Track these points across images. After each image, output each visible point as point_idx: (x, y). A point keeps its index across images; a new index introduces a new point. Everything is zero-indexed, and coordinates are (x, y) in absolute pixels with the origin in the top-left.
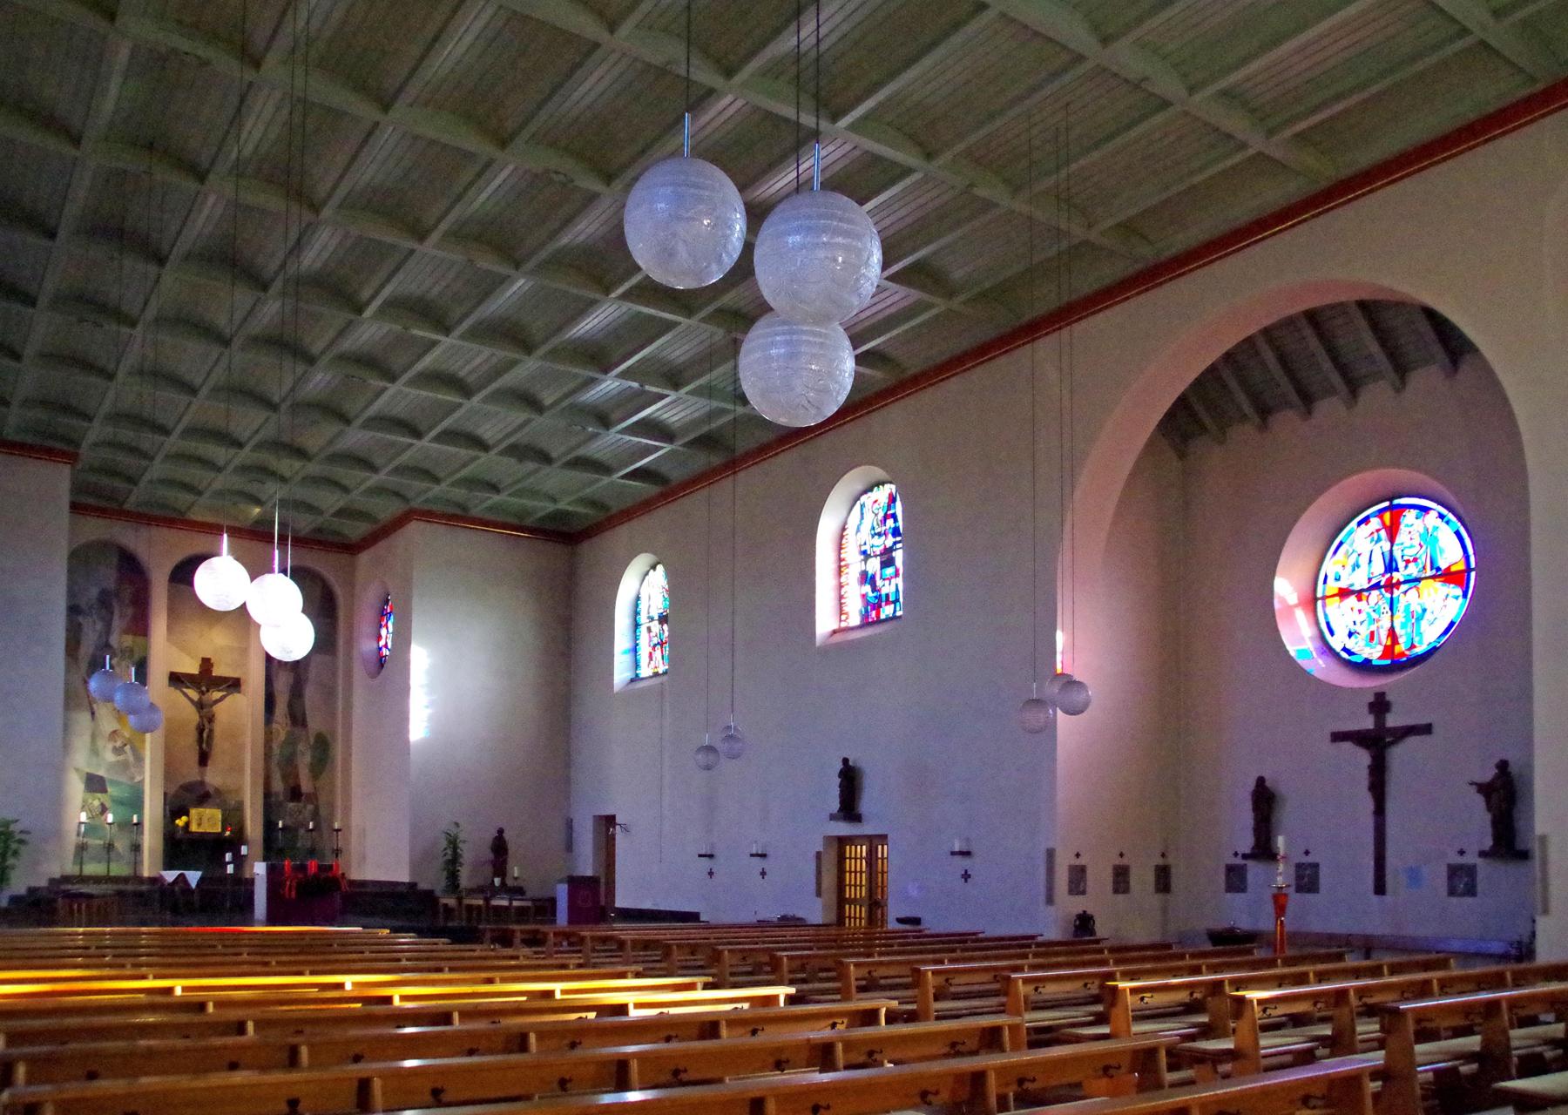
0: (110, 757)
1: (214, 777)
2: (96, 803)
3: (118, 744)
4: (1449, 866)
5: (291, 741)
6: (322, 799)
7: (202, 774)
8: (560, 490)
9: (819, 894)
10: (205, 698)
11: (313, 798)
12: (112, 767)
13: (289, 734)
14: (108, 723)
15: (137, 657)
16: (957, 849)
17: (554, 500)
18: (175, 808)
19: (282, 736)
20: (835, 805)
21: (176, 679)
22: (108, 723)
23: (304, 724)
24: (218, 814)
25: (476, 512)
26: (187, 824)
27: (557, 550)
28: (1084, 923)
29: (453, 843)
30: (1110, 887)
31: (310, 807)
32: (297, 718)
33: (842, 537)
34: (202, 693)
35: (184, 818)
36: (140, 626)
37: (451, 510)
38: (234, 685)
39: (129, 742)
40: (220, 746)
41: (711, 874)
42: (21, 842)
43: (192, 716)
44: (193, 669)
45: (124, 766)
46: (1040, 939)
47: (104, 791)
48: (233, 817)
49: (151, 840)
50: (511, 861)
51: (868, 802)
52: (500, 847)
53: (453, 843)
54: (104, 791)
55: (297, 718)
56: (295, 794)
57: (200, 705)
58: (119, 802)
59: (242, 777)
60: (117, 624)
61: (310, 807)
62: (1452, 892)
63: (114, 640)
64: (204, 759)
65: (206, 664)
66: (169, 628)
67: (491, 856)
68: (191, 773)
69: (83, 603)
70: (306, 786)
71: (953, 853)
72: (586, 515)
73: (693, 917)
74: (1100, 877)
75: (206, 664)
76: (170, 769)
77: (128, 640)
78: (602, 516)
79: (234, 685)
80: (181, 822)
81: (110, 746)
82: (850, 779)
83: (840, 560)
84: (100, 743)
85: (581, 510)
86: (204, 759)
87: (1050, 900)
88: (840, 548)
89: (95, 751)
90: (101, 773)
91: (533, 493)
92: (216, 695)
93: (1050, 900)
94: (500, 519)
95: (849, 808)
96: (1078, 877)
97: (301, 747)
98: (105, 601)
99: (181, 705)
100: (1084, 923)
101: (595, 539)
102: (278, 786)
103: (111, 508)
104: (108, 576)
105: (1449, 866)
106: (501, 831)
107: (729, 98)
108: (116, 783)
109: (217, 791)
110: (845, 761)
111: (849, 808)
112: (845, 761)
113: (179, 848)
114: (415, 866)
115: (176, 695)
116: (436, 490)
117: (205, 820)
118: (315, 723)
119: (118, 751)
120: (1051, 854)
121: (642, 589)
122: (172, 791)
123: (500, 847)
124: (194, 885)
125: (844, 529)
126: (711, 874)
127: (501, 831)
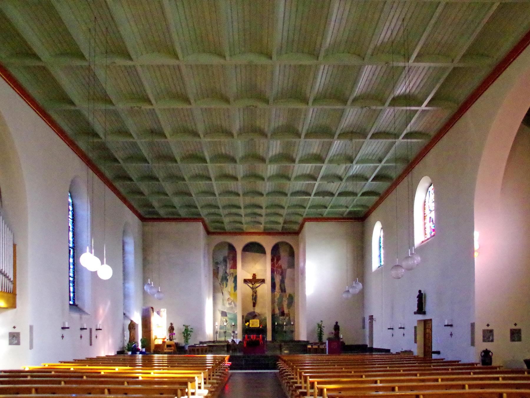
0: (228, 306)
1: (257, 310)
2: (224, 320)
3: (230, 302)
4: (511, 330)
5: (281, 297)
6: (291, 315)
7: (254, 309)
8: (348, 204)
9: (416, 342)
10: (254, 286)
11: (288, 315)
12: (229, 309)
13: (280, 295)
14: (227, 296)
15: (234, 275)
16: (446, 324)
17: (347, 207)
18: (246, 319)
19: (278, 296)
20: (416, 309)
21: (246, 281)
22: (227, 296)
23: (285, 292)
24: (258, 321)
25: (325, 215)
26: (249, 325)
27: (358, 224)
28: (486, 356)
29: (320, 327)
30: (509, 338)
31: (287, 318)
32: (283, 290)
33: (425, 205)
34: (253, 285)
35: (248, 323)
36: (234, 266)
37: (337, 216)
38: (263, 281)
39: (233, 301)
40: (259, 299)
41: (451, 335)
42: (191, 331)
43: (250, 291)
44: (250, 277)
45: (232, 308)
46: (460, 363)
47: (226, 316)
48: (263, 322)
49: (239, 330)
50: (340, 332)
51: (429, 306)
52: (337, 328)
53: (320, 327)
54: (226, 316)
55: (283, 290)
56: (283, 314)
57: (252, 288)
58: (231, 319)
59: (265, 309)
60: (229, 266)
61: (287, 318)
62: (492, 341)
63: (228, 271)
64: (254, 305)
65: (254, 275)
66: (243, 266)
67: (333, 331)
68: (251, 309)
69: (218, 261)
70: (286, 311)
71: (445, 326)
72: (362, 211)
73: (388, 351)
74: (502, 335)
75: (254, 275)
76: (244, 309)
77: (232, 271)
78: (367, 210)
79: (263, 281)
80: (247, 324)
81: (228, 302)
82: (421, 297)
83: (425, 214)
84: (225, 302)
85: (359, 209)
86: (254, 305)
87: (473, 344)
88: (424, 209)
89: (224, 304)
90: (225, 311)
91: (341, 206)
92: (257, 285)
93: (473, 344)
94: (333, 217)
95: (421, 310)
96: (488, 335)
97: (284, 299)
98: (225, 260)
99: (247, 289)
100: (486, 356)
101: (368, 218)
102: (277, 311)
103: (223, 232)
104: (225, 252)
105: (511, 330)
106: (337, 323)
107: (322, 67)
108: (230, 313)
109: (259, 315)
110: (420, 291)
111: (421, 310)
112: (420, 291)
113: (247, 331)
114: (308, 337)
115: (246, 286)
116: (327, 210)
117: (255, 323)
118: (288, 291)
119: (230, 304)
120: (473, 325)
121: (377, 232)
122: (245, 315)
123: (337, 328)
124: (237, 343)
125: (425, 202)
126: (451, 335)
127: (337, 323)
